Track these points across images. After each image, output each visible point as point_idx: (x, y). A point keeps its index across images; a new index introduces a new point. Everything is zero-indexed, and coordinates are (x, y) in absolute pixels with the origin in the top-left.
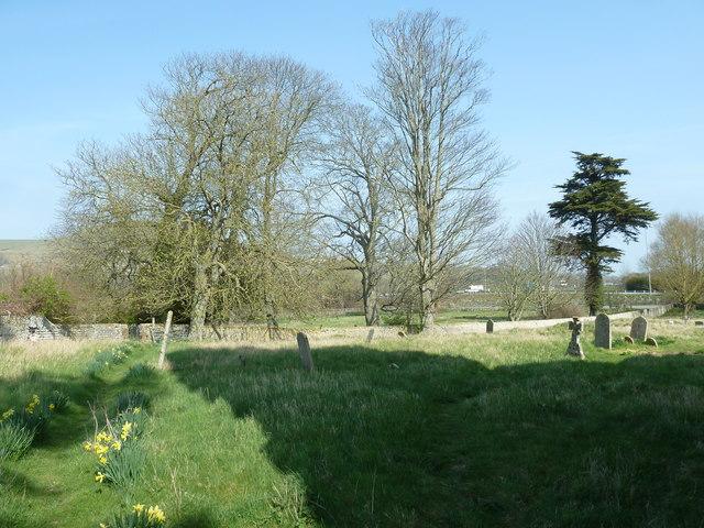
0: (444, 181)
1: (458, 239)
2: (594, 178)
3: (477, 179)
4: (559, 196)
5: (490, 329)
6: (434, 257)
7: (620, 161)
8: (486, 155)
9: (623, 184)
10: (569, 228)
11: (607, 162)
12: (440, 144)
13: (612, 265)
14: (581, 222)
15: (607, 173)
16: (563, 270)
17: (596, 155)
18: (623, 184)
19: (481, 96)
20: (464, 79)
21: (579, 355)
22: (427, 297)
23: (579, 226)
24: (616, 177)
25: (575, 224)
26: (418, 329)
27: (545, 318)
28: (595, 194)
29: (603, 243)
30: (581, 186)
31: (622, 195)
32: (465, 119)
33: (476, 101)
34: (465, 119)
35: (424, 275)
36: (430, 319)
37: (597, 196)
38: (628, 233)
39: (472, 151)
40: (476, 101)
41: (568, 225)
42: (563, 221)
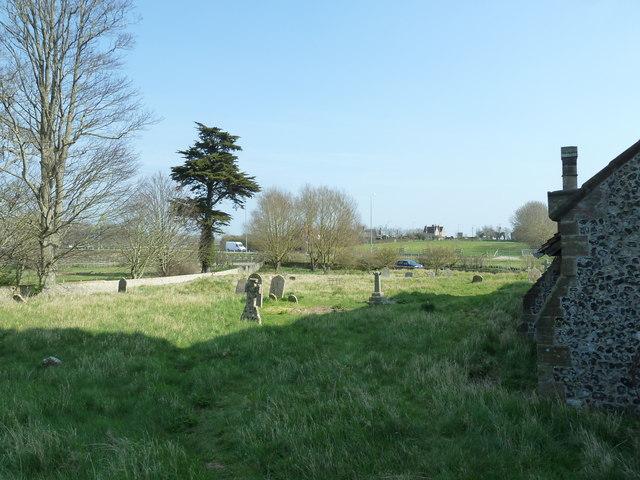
0: (76, 124)
1: (89, 192)
2: (212, 149)
3: (118, 127)
4: (181, 162)
5: (122, 287)
6: (60, 209)
7: (235, 138)
8: (127, 104)
9: (236, 158)
10: (189, 192)
11: (224, 137)
12: (75, 82)
13: (223, 227)
14: (198, 187)
15: (224, 147)
16: (181, 231)
17: (215, 129)
18: (236, 158)
19: (125, 41)
20: (110, 16)
21: (257, 319)
22: (49, 253)
23: (196, 190)
24: (231, 152)
25: (193, 189)
26: (33, 290)
27: (164, 275)
28: (213, 163)
29: (216, 208)
30: (200, 155)
31: (234, 167)
32: (102, 61)
33: (118, 45)
34: (102, 61)
35: (47, 228)
36: (51, 278)
37: (212, 164)
38: (236, 201)
39: (111, 97)
40: (118, 45)
41: (187, 188)
42: (183, 185)
